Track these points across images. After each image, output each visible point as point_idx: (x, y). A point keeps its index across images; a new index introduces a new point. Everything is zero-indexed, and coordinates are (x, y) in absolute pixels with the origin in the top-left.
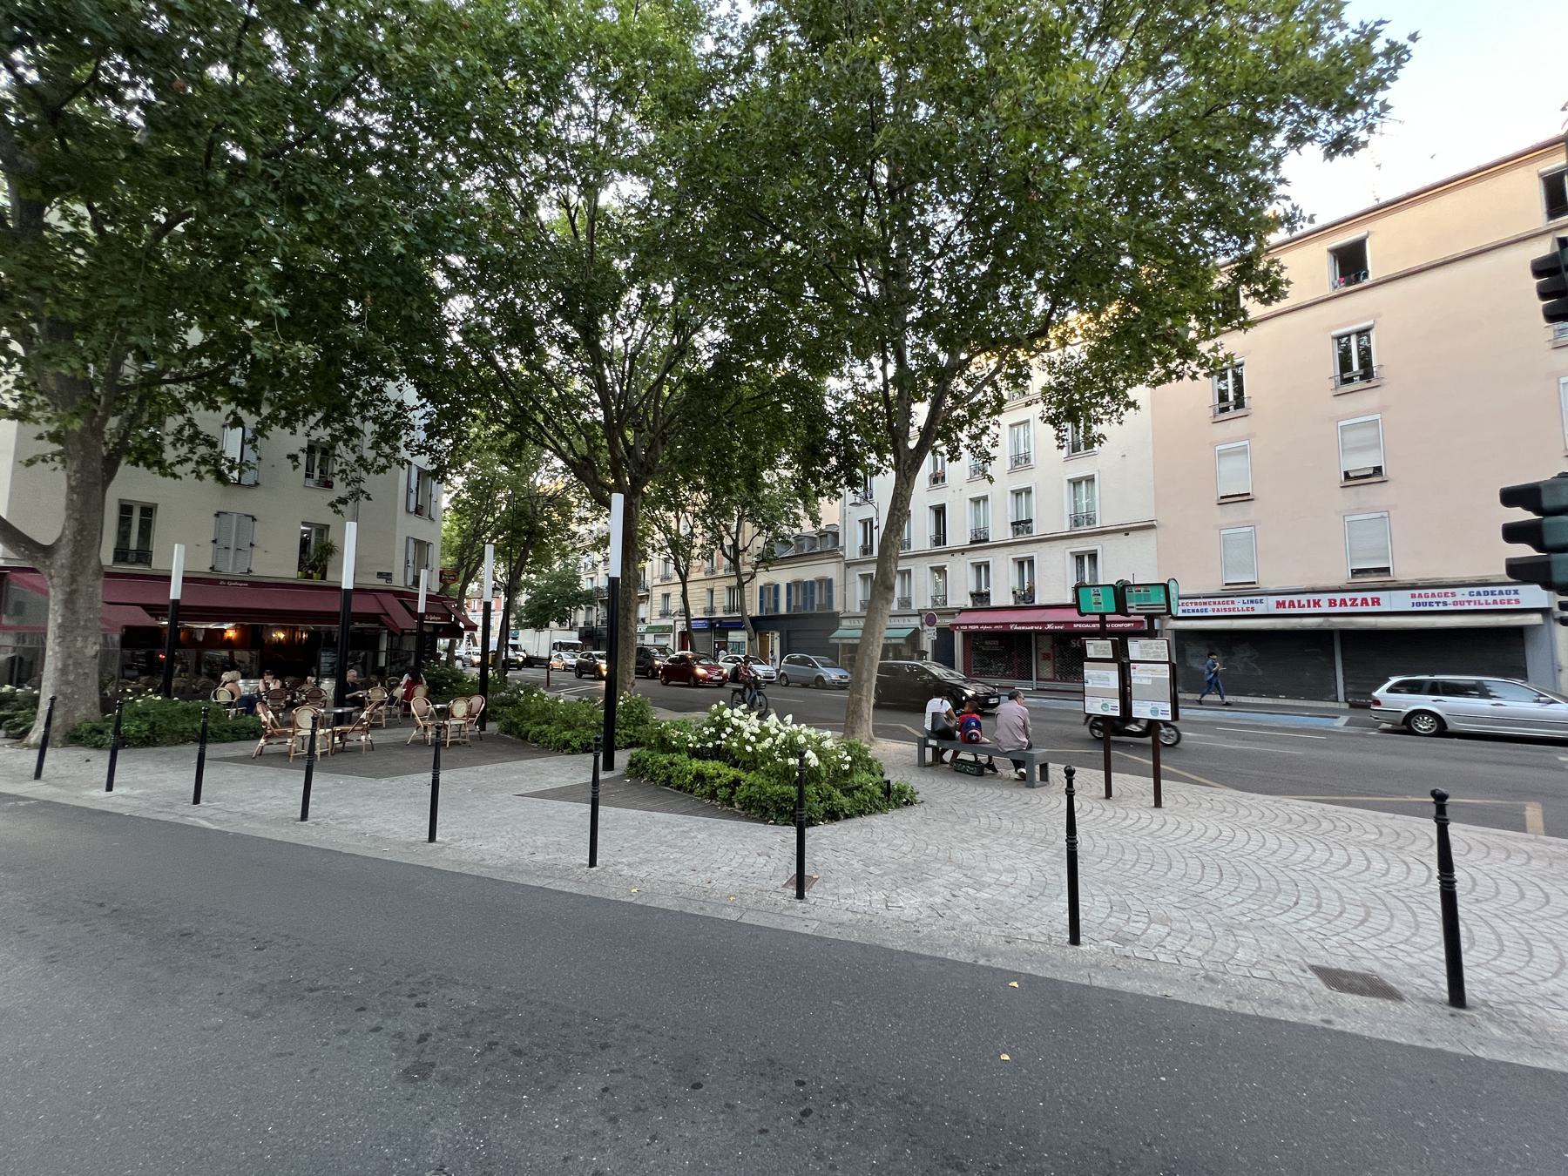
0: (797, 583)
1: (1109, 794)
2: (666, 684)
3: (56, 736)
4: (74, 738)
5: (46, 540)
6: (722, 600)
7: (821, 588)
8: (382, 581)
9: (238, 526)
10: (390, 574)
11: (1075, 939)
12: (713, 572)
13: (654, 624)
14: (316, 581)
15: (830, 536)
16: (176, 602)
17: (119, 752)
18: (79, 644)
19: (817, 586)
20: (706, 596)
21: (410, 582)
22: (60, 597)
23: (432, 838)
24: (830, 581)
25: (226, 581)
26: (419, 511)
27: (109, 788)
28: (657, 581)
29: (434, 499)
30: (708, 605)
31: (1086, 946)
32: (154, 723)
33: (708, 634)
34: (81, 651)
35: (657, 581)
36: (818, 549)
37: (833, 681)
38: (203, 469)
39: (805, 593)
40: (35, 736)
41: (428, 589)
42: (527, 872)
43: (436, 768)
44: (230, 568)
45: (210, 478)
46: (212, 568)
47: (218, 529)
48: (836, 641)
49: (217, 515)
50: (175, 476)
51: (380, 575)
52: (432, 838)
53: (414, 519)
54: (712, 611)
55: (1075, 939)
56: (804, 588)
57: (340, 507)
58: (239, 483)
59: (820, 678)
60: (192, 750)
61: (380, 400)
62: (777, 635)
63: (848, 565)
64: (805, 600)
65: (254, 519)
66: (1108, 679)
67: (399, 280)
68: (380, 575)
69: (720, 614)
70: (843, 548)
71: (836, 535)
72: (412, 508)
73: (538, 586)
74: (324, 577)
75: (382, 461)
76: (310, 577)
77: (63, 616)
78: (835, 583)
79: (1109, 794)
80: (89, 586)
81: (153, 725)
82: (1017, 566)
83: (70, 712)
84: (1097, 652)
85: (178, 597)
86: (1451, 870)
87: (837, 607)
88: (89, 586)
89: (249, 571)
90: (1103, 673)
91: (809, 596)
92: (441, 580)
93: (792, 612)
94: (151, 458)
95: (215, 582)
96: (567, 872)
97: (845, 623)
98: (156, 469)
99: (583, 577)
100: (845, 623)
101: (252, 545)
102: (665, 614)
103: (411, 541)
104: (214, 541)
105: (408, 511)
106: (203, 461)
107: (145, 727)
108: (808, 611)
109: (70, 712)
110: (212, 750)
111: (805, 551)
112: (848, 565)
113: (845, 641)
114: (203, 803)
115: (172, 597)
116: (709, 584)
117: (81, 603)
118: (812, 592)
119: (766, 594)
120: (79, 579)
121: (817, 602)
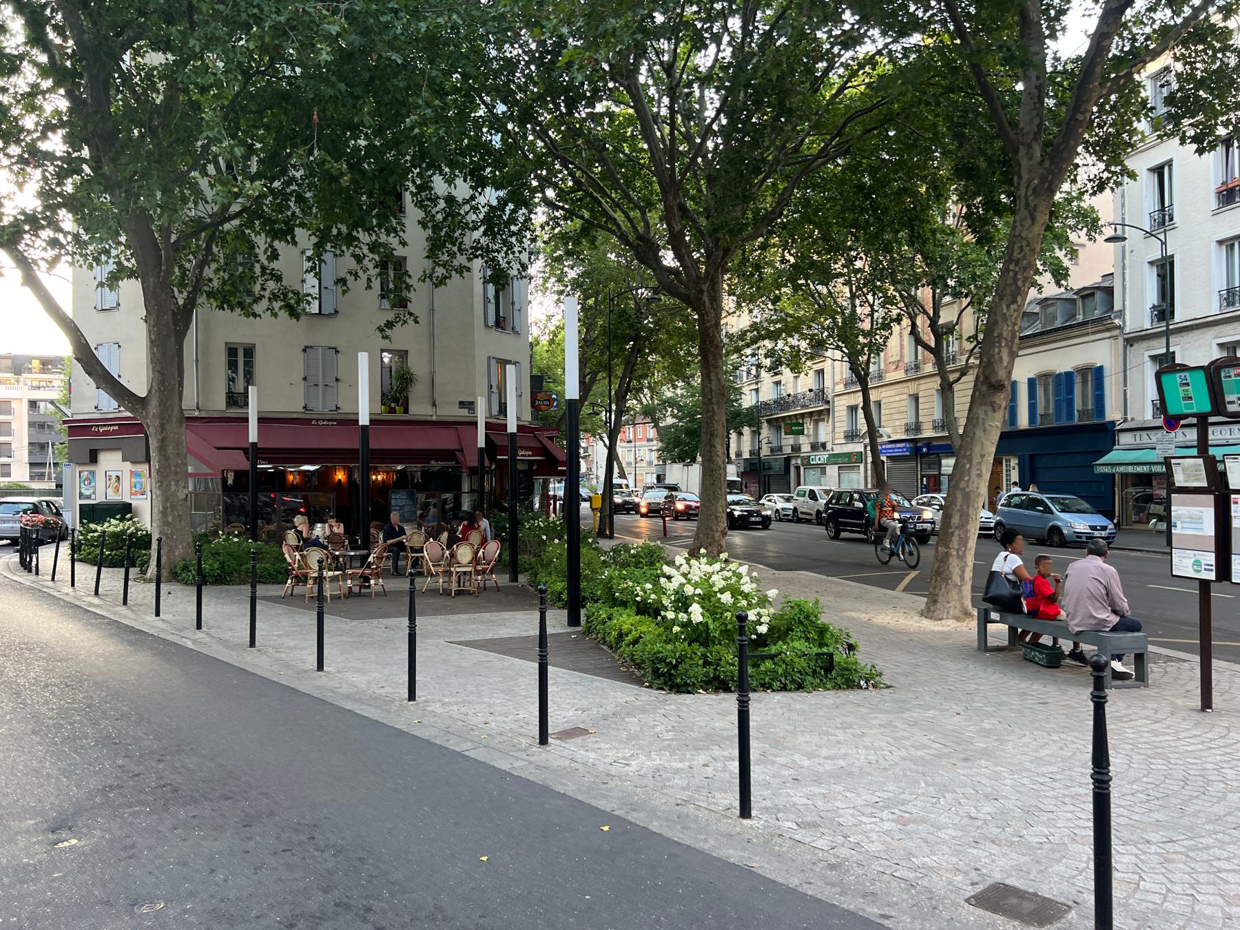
0: (1045, 376)
1: (1207, 702)
2: (836, 537)
3: (164, 573)
4: (175, 577)
5: (142, 393)
6: (931, 410)
7: (1084, 382)
8: (464, 412)
9: (323, 360)
10: (472, 403)
11: (745, 810)
12: (917, 367)
13: (838, 450)
14: (400, 416)
15: (1098, 295)
16: (254, 444)
17: (203, 587)
18: (173, 488)
19: (1078, 379)
20: (907, 405)
21: (495, 411)
22: (156, 445)
23: (320, 666)
24: (1100, 370)
25: (317, 420)
26: (500, 323)
27: (158, 614)
28: (840, 388)
29: (516, 307)
30: (911, 419)
31: (758, 821)
32: (224, 562)
33: (913, 464)
34: (174, 495)
35: (840, 388)
36: (1080, 318)
37: (1079, 535)
38: (277, 305)
39: (1057, 393)
40: (152, 570)
41: (518, 419)
42: (360, 701)
43: (412, 619)
44: (321, 407)
45: (284, 315)
46: (305, 407)
47: (307, 366)
48: (1107, 470)
49: (304, 350)
50: (255, 315)
51: (462, 404)
52: (320, 666)
53: (495, 334)
54: (918, 427)
55: (745, 810)
56: (1064, 382)
57: (388, 332)
58: (320, 313)
59: (1056, 530)
60: (247, 589)
61: (428, 199)
62: (1014, 462)
63: (1130, 341)
64: (1057, 403)
65: (337, 352)
66: (1199, 520)
67: (342, 86)
68: (462, 404)
69: (928, 433)
70: (1121, 314)
71: (1109, 291)
72: (492, 320)
73: (686, 405)
74: (406, 411)
75: (440, 271)
76: (392, 411)
77: (159, 462)
78: (1106, 373)
79: (1207, 702)
80: (175, 433)
81: (222, 563)
82: (1136, 346)
83: (171, 551)
84: (1187, 477)
85: (256, 441)
86: (740, 712)
87: (1112, 413)
88: (175, 433)
89: (338, 408)
90: (1194, 510)
91: (1063, 396)
92: (533, 405)
93: (1038, 425)
94: (234, 301)
95: (307, 422)
96: (382, 702)
97: (1125, 439)
98: (238, 310)
99: (746, 390)
100: (1125, 439)
101: (337, 380)
102: (851, 436)
103: (493, 362)
104: (305, 379)
105: (486, 325)
106: (274, 297)
107: (216, 565)
108: (1064, 422)
109: (171, 551)
110: (261, 590)
111: (1058, 324)
112: (1130, 341)
113: (1122, 469)
114: (204, 629)
115: (250, 441)
116: (912, 388)
117: (170, 448)
118: (1070, 391)
119: (1040, 391)
120: (167, 427)
121: (1078, 405)
